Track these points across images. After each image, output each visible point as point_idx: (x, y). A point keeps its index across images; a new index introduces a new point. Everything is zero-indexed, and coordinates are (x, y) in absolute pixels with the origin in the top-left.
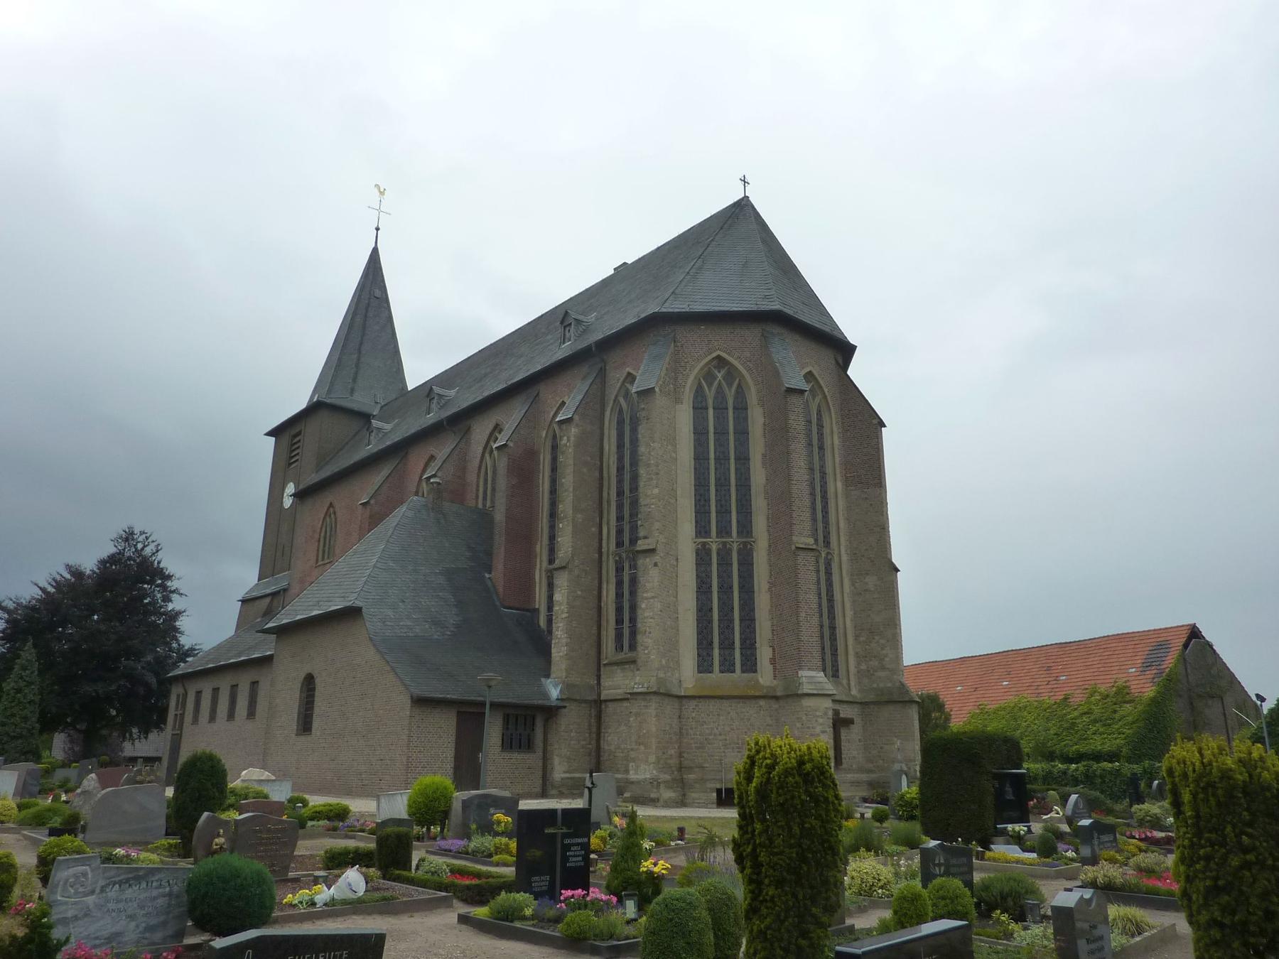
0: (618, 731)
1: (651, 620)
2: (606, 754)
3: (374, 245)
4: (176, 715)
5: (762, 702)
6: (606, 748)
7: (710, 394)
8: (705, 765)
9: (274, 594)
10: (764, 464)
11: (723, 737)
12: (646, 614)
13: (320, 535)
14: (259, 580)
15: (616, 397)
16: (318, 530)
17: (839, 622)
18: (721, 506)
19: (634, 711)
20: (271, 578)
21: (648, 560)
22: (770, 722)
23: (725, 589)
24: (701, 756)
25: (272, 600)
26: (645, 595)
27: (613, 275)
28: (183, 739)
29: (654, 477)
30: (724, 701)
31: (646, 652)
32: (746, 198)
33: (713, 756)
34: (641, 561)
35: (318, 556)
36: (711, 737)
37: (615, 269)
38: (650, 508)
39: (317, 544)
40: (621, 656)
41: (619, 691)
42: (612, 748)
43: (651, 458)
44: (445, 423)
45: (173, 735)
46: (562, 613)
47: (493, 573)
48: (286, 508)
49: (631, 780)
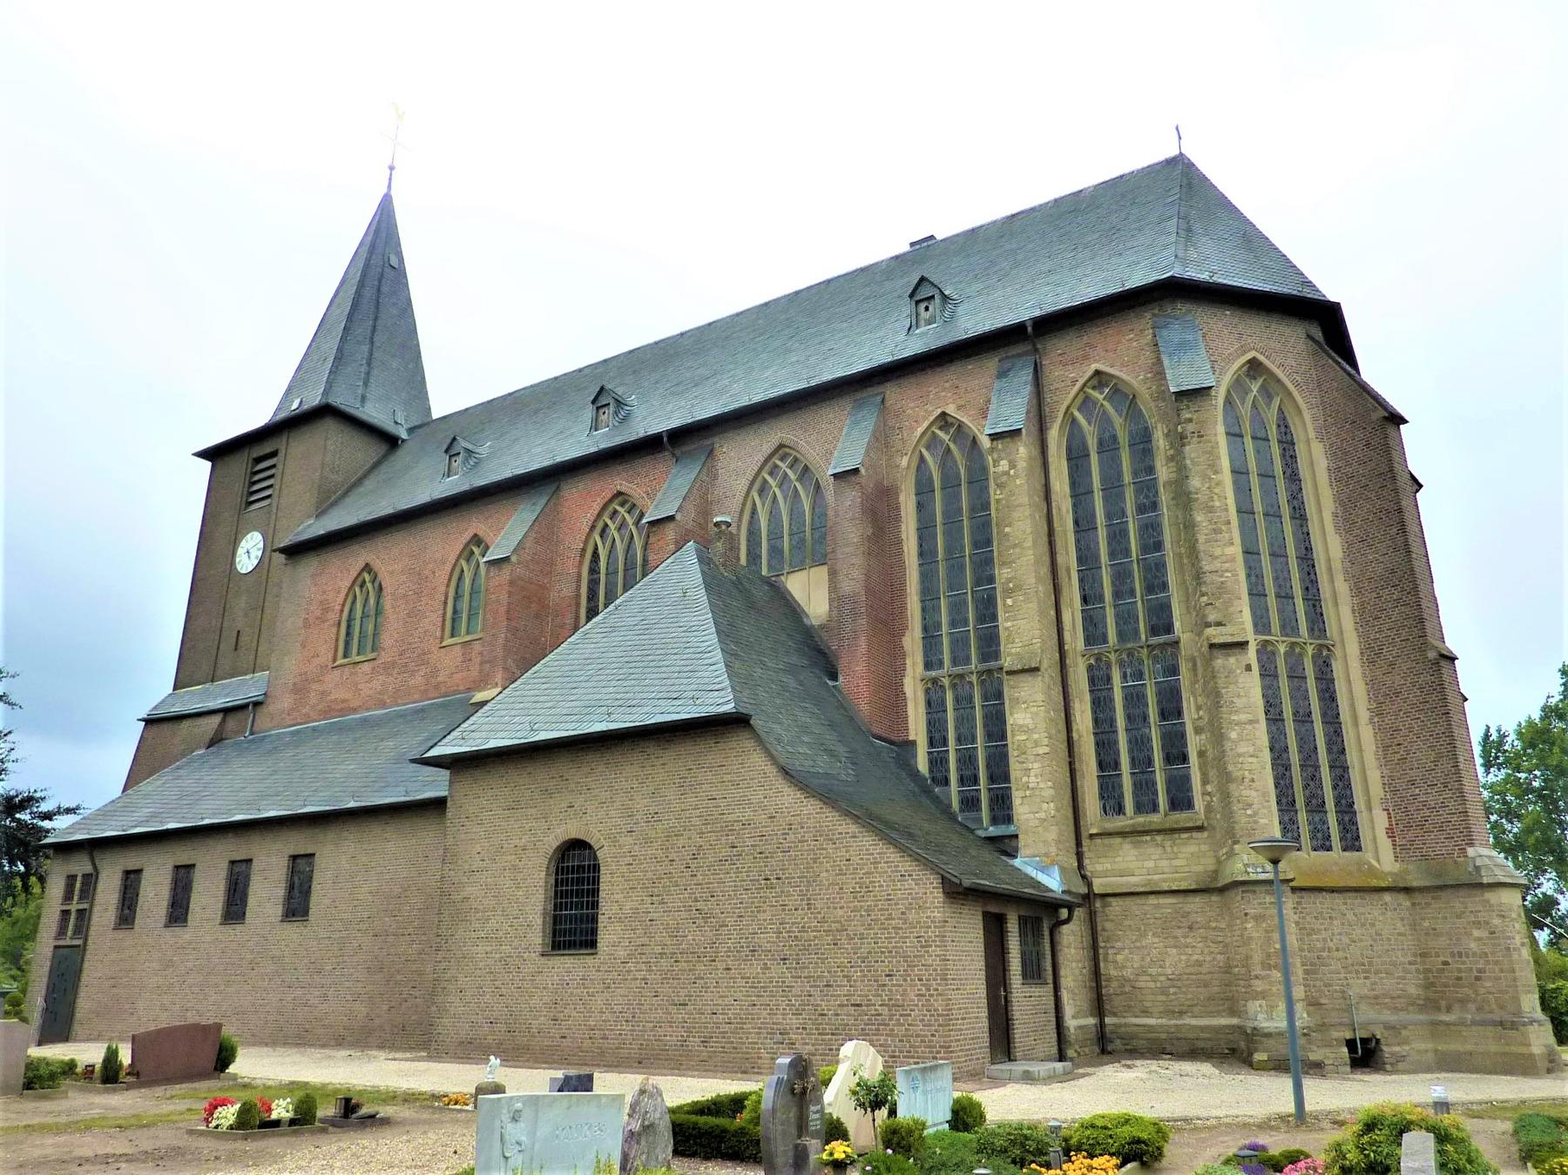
0: (1138, 944)
1: (1250, 760)
2: (1114, 984)
3: (385, 191)
4: (66, 913)
5: (1387, 897)
6: (1113, 973)
7: (1245, 411)
8: (1323, 1001)
9: (226, 711)
10: (1337, 528)
11: (1341, 954)
12: (1241, 750)
13: (341, 616)
14: (176, 688)
15: (1068, 408)
16: (338, 608)
17: (1352, 757)
18: (1280, 586)
19: (1251, 911)
20: (207, 685)
21: (1232, 660)
22: (1402, 930)
23: (1303, 718)
24: (1314, 986)
25: (223, 721)
26: (1235, 717)
27: (904, 254)
28: (88, 956)
29: (1223, 527)
30: (1336, 895)
31: (1249, 812)
32: (1181, 154)
33: (1330, 985)
34: (1219, 661)
35: (336, 650)
36: (1325, 954)
37: (912, 244)
38: (1222, 576)
39: (334, 630)
40: (1119, 823)
41: (1132, 879)
42: (1128, 973)
43: (1216, 497)
44: (665, 439)
45: (56, 947)
46: (1037, 744)
47: (841, 678)
48: (243, 571)
49: (1266, 1031)
